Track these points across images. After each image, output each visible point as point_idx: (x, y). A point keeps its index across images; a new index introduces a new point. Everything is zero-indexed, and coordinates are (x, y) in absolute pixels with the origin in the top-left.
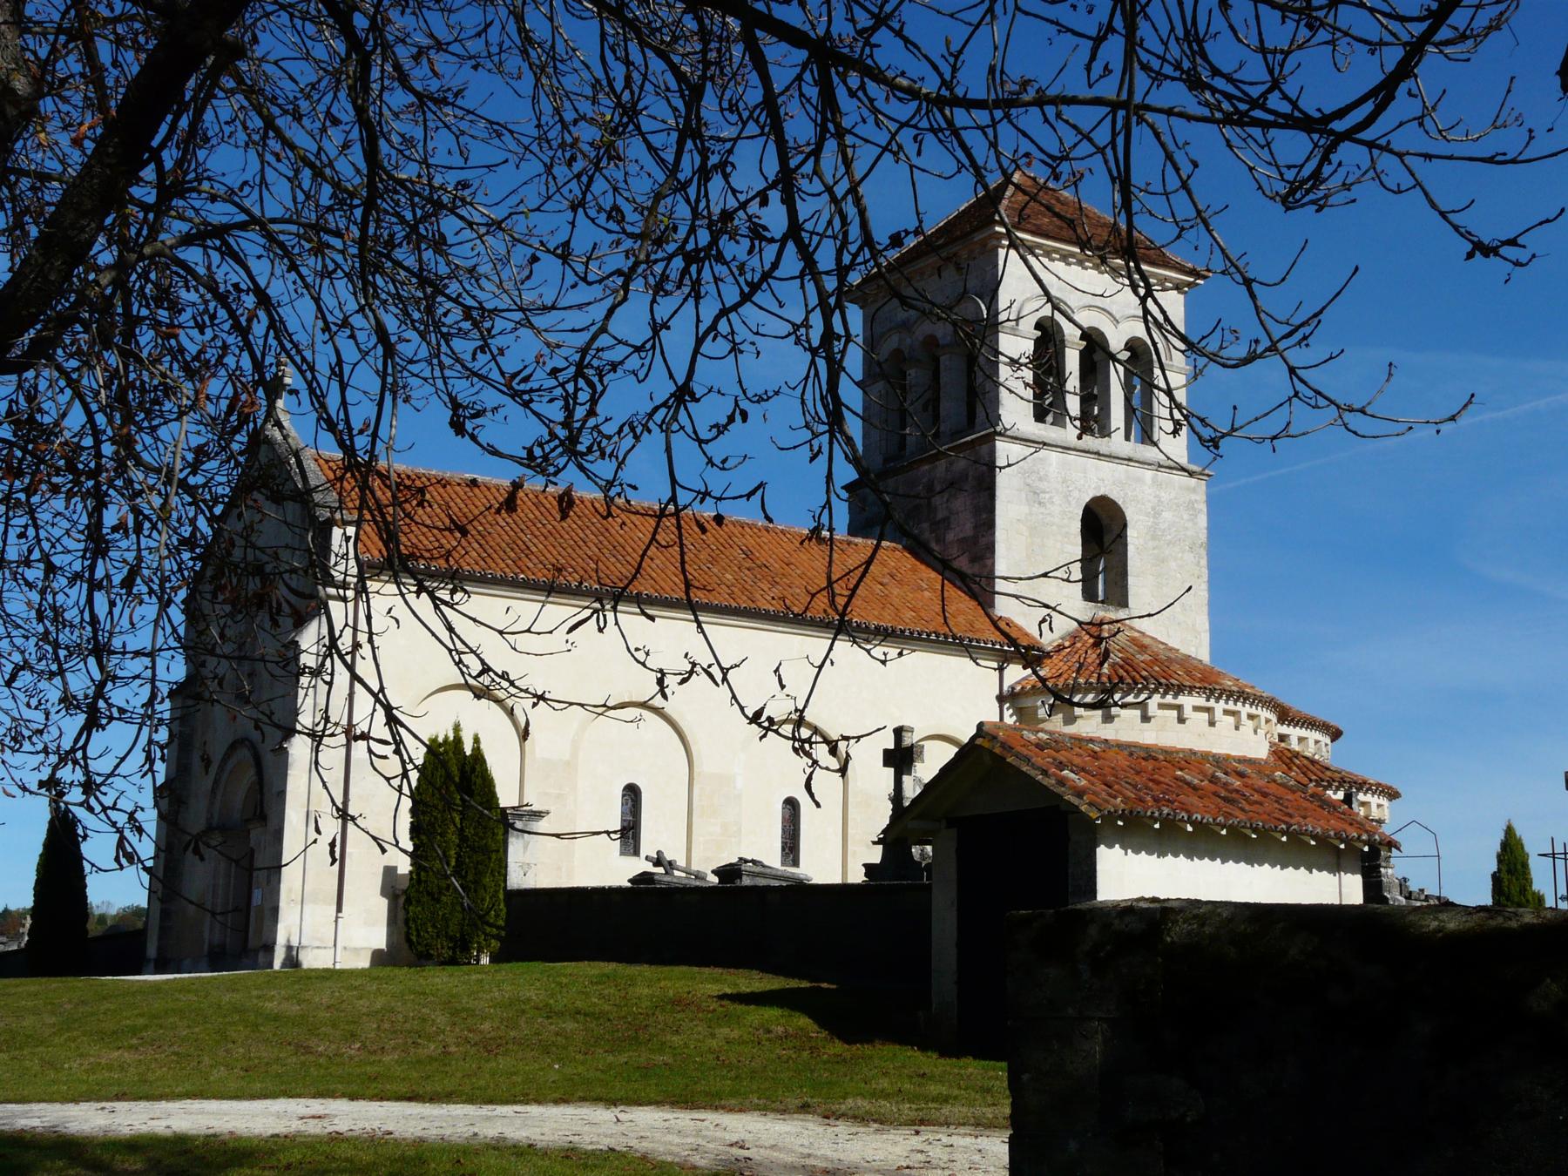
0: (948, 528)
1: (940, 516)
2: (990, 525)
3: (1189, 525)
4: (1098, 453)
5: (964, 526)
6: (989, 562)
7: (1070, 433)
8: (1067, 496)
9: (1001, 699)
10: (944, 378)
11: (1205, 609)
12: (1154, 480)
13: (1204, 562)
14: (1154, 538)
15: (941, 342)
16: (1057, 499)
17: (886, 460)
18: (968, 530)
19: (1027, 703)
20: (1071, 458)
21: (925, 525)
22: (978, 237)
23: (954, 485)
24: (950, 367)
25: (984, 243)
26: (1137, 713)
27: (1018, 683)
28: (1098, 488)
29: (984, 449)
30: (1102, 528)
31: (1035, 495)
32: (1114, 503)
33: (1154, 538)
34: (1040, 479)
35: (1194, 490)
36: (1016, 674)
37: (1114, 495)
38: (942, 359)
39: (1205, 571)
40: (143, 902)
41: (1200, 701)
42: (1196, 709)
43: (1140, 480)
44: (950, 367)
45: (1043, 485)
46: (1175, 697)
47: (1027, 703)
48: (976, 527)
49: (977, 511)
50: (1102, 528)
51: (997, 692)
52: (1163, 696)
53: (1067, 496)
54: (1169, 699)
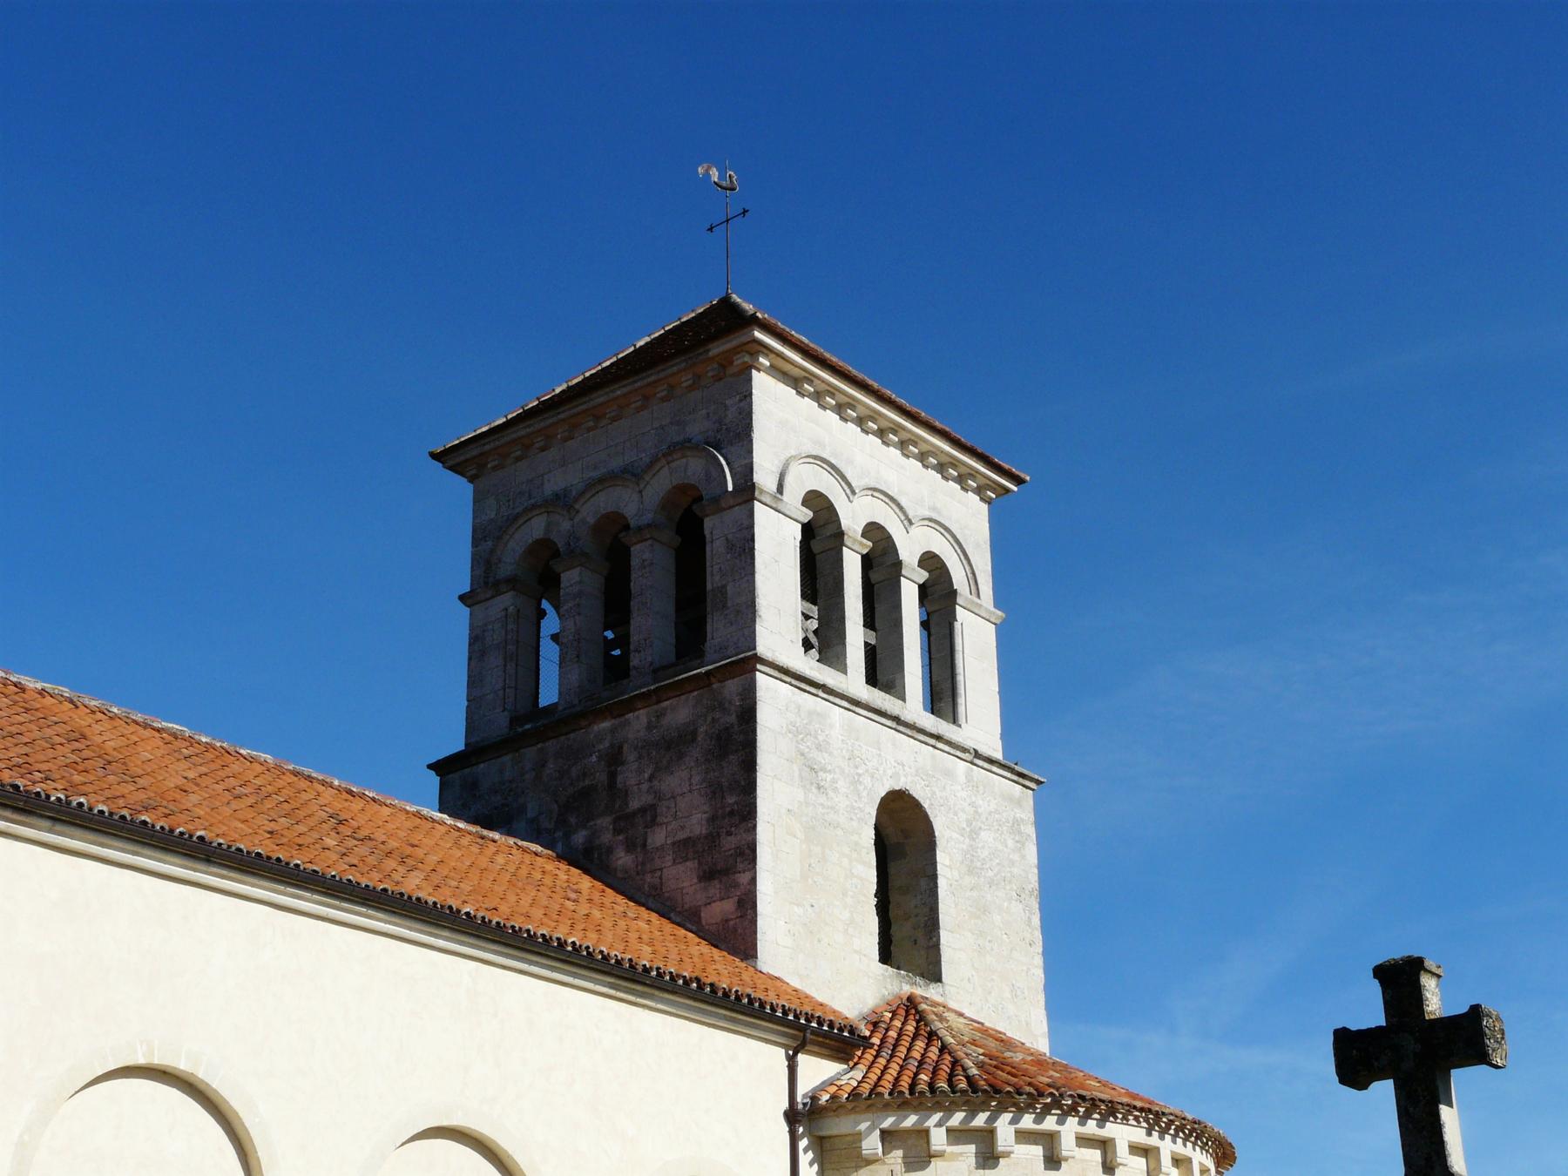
0: (653, 823)
1: (634, 804)
2: (746, 813)
3: (1016, 857)
4: (896, 719)
5: (690, 814)
6: (744, 878)
7: (854, 680)
8: (856, 782)
9: (792, 1116)
10: (637, 581)
11: (1041, 998)
12: (969, 777)
13: (1036, 921)
14: (971, 871)
15: (633, 523)
16: (842, 785)
17: (515, 721)
18: (696, 824)
19: (837, 1126)
20: (860, 721)
21: (605, 822)
22: (717, 349)
23: (674, 746)
24: (652, 569)
25: (725, 361)
26: (1037, 1151)
27: (822, 1087)
28: (895, 776)
29: (732, 687)
30: (903, 840)
31: (812, 774)
32: (916, 805)
33: (971, 871)
34: (819, 747)
35: (1019, 803)
36: (816, 1071)
37: (918, 793)
38: (635, 549)
39: (1038, 935)
40: (1383, 1023)
41: (1137, 1134)
42: (1136, 1149)
43: (949, 774)
44: (652, 569)
45: (822, 758)
46: (1101, 1123)
47: (837, 1126)
48: (713, 819)
49: (715, 791)
50: (903, 840)
51: (785, 1105)
52: (1082, 1123)
53: (856, 782)
54: (1091, 1127)
